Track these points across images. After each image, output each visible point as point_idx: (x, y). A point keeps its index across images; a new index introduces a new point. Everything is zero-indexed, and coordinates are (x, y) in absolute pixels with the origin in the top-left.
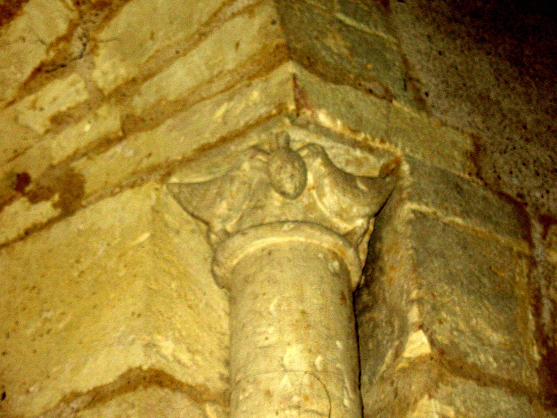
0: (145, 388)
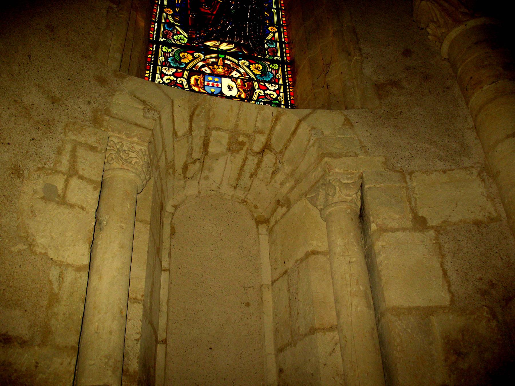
0: (310, 256)
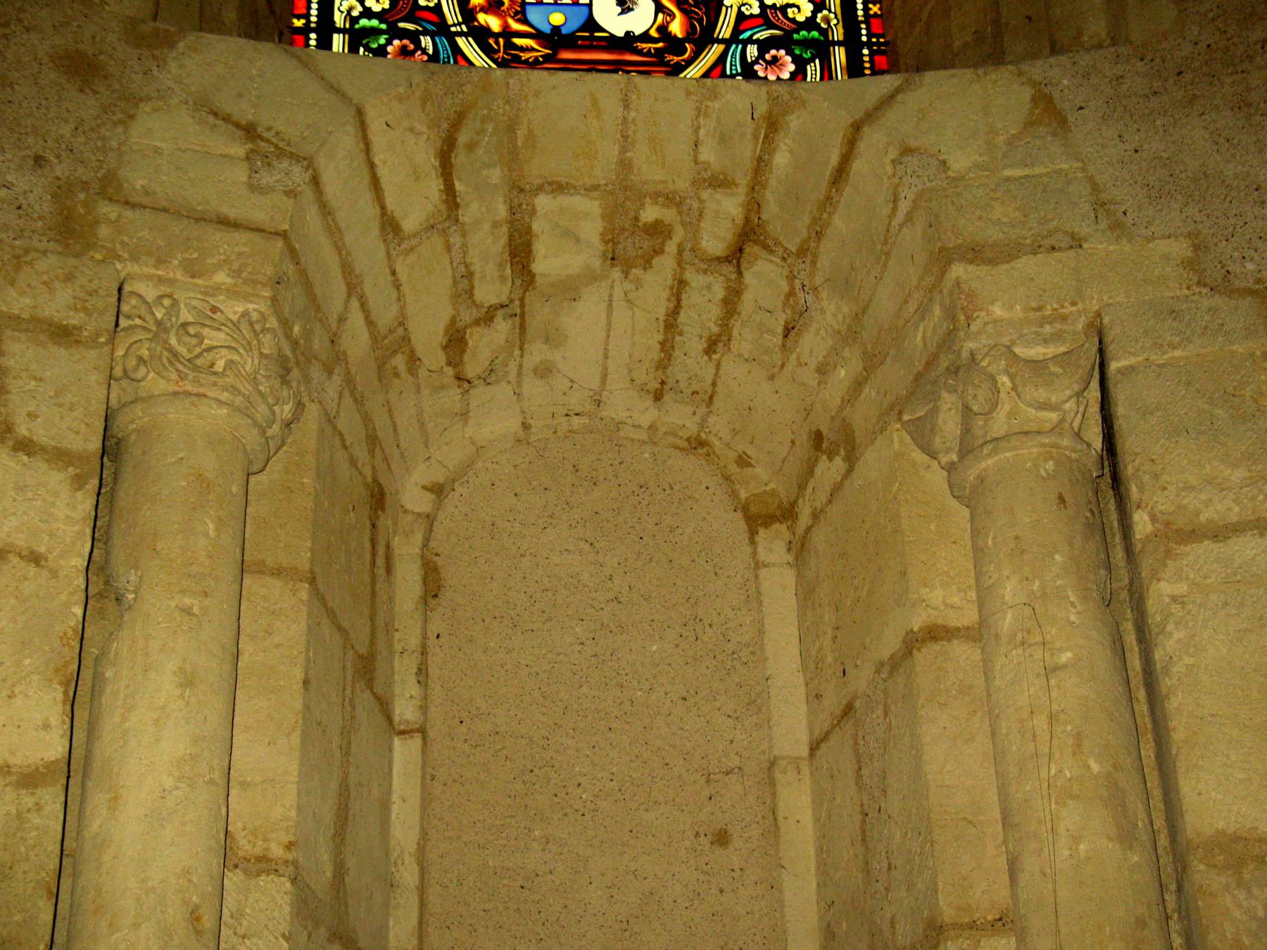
0: (919, 649)
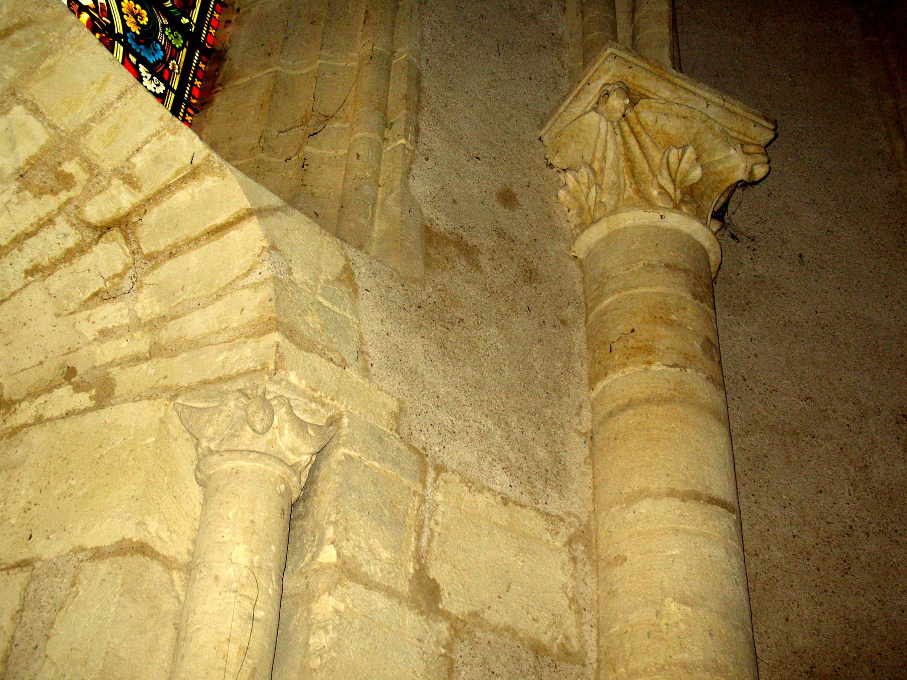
0: (132, 555)
